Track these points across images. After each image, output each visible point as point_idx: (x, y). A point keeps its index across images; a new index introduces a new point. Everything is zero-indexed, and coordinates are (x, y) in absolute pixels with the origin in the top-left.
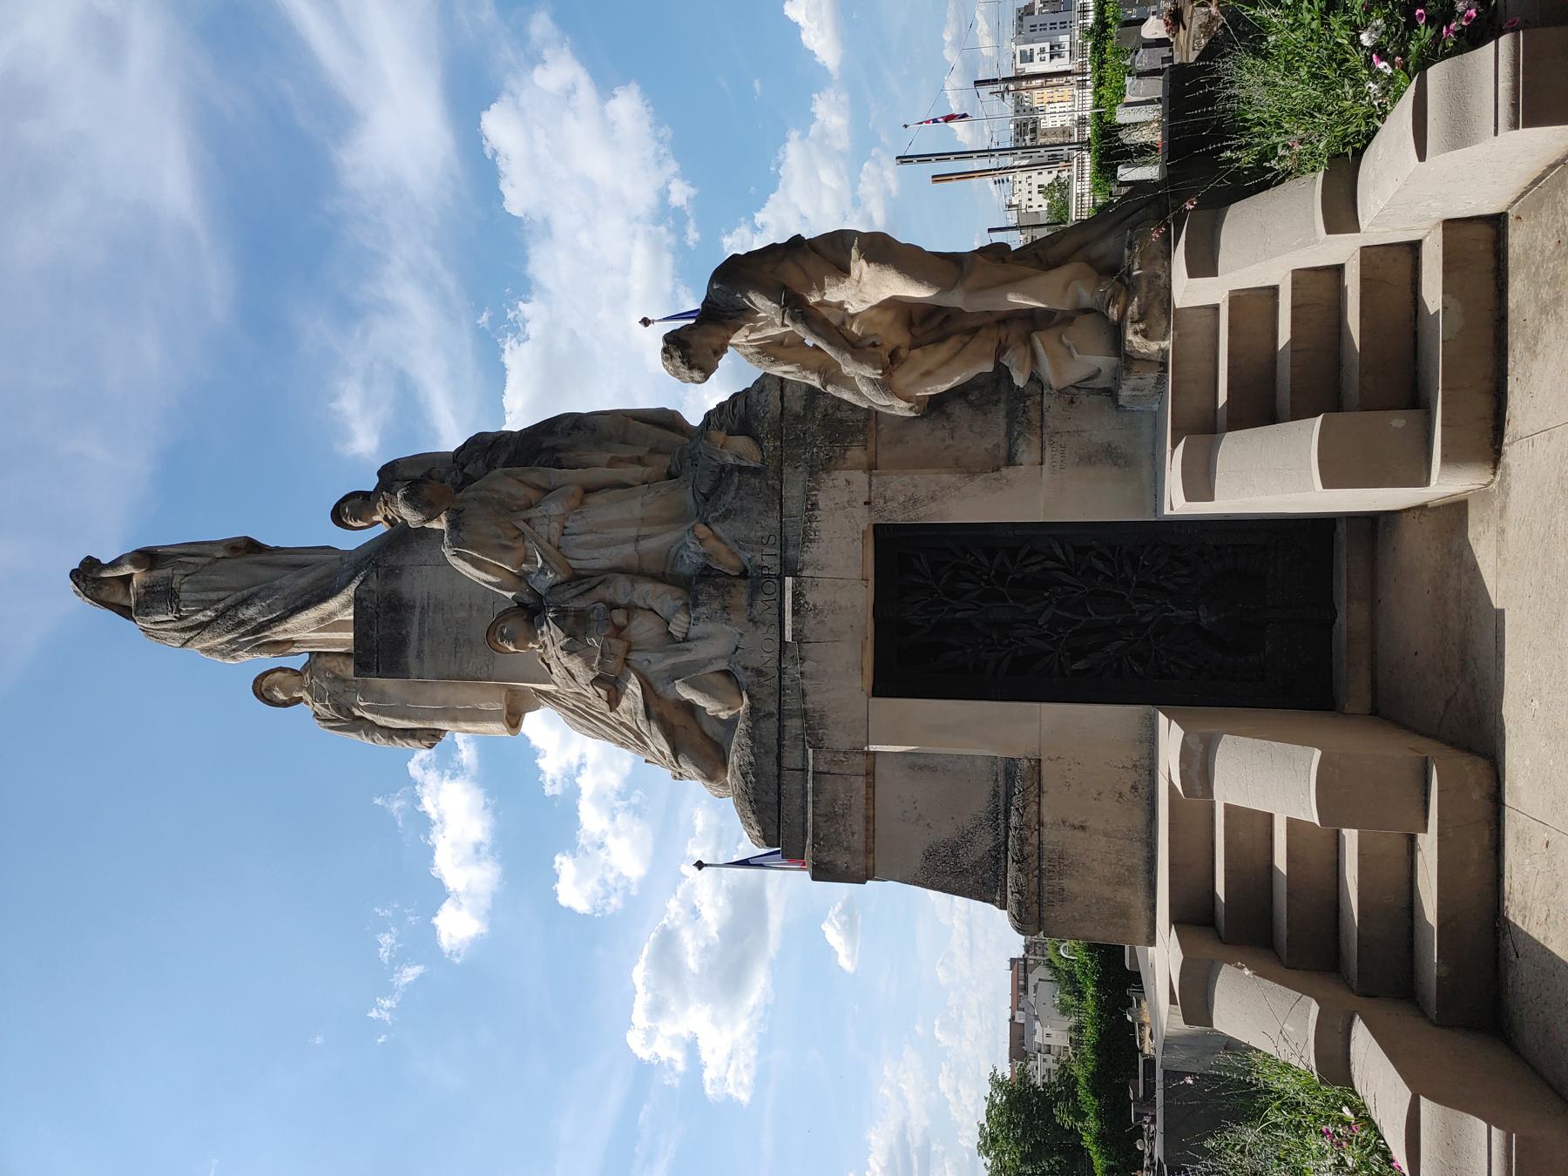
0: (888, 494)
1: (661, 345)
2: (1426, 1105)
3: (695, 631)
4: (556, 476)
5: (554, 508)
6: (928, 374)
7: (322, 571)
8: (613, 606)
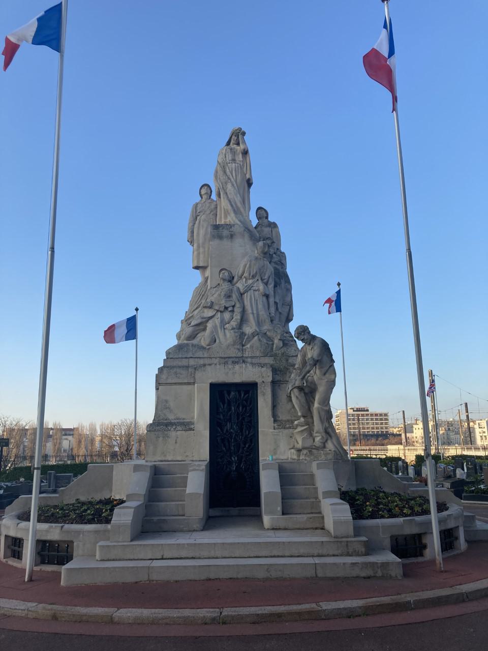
0: (266, 388)
2: (133, 510)
3: (227, 331)
4: (271, 286)
5: (261, 287)
6: (297, 397)
7: (242, 209)
8: (233, 306)
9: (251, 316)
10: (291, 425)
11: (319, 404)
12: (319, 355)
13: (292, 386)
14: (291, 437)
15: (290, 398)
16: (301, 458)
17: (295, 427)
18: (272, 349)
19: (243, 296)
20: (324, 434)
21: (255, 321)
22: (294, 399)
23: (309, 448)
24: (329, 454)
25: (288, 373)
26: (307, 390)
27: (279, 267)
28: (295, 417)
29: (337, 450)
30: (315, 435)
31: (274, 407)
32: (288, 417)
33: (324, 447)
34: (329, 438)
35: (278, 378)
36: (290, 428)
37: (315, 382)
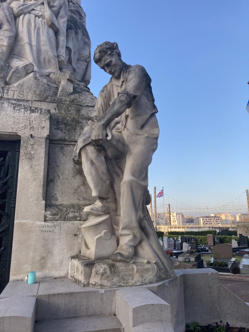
0: (36, 146)
1: (112, 42)
5: (47, 13)
6: (92, 163)
9: (27, 48)
10: (77, 214)
11: (133, 174)
12: (137, 88)
13: (85, 140)
14: (75, 235)
15: (78, 163)
16: (92, 281)
17: (84, 217)
18: (56, 94)
19: (18, 19)
20: (137, 231)
21: (33, 56)
22: (86, 167)
23: (108, 258)
24: (147, 270)
25: (78, 128)
26: (110, 153)
27: (76, 17)
28: (84, 199)
29: (159, 261)
30: (120, 231)
31: (49, 181)
32: (74, 200)
33: (136, 254)
34: (144, 237)
35: (60, 135)
36: (75, 218)
37: (124, 140)
